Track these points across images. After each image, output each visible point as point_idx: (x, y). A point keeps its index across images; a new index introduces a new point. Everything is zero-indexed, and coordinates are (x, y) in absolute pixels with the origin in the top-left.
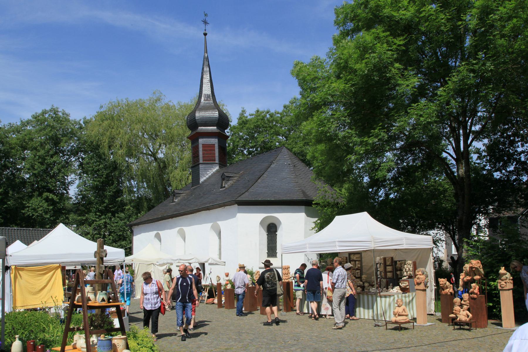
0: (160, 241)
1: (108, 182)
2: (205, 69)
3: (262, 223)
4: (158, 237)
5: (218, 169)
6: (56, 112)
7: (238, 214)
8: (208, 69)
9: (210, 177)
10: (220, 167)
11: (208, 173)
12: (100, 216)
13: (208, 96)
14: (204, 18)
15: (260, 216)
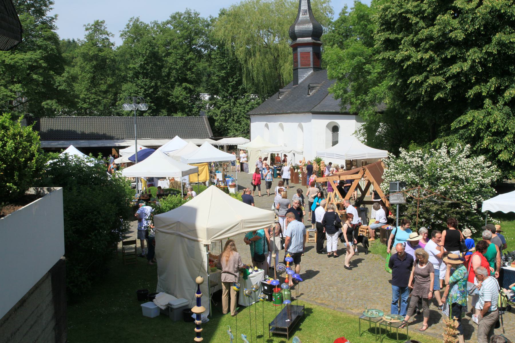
0: (268, 129)
1: (231, 74)
3: (328, 126)
4: (267, 126)
6: (189, 14)
9: (306, 79)
10: (314, 70)
12: (226, 101)
15: (327, 121)
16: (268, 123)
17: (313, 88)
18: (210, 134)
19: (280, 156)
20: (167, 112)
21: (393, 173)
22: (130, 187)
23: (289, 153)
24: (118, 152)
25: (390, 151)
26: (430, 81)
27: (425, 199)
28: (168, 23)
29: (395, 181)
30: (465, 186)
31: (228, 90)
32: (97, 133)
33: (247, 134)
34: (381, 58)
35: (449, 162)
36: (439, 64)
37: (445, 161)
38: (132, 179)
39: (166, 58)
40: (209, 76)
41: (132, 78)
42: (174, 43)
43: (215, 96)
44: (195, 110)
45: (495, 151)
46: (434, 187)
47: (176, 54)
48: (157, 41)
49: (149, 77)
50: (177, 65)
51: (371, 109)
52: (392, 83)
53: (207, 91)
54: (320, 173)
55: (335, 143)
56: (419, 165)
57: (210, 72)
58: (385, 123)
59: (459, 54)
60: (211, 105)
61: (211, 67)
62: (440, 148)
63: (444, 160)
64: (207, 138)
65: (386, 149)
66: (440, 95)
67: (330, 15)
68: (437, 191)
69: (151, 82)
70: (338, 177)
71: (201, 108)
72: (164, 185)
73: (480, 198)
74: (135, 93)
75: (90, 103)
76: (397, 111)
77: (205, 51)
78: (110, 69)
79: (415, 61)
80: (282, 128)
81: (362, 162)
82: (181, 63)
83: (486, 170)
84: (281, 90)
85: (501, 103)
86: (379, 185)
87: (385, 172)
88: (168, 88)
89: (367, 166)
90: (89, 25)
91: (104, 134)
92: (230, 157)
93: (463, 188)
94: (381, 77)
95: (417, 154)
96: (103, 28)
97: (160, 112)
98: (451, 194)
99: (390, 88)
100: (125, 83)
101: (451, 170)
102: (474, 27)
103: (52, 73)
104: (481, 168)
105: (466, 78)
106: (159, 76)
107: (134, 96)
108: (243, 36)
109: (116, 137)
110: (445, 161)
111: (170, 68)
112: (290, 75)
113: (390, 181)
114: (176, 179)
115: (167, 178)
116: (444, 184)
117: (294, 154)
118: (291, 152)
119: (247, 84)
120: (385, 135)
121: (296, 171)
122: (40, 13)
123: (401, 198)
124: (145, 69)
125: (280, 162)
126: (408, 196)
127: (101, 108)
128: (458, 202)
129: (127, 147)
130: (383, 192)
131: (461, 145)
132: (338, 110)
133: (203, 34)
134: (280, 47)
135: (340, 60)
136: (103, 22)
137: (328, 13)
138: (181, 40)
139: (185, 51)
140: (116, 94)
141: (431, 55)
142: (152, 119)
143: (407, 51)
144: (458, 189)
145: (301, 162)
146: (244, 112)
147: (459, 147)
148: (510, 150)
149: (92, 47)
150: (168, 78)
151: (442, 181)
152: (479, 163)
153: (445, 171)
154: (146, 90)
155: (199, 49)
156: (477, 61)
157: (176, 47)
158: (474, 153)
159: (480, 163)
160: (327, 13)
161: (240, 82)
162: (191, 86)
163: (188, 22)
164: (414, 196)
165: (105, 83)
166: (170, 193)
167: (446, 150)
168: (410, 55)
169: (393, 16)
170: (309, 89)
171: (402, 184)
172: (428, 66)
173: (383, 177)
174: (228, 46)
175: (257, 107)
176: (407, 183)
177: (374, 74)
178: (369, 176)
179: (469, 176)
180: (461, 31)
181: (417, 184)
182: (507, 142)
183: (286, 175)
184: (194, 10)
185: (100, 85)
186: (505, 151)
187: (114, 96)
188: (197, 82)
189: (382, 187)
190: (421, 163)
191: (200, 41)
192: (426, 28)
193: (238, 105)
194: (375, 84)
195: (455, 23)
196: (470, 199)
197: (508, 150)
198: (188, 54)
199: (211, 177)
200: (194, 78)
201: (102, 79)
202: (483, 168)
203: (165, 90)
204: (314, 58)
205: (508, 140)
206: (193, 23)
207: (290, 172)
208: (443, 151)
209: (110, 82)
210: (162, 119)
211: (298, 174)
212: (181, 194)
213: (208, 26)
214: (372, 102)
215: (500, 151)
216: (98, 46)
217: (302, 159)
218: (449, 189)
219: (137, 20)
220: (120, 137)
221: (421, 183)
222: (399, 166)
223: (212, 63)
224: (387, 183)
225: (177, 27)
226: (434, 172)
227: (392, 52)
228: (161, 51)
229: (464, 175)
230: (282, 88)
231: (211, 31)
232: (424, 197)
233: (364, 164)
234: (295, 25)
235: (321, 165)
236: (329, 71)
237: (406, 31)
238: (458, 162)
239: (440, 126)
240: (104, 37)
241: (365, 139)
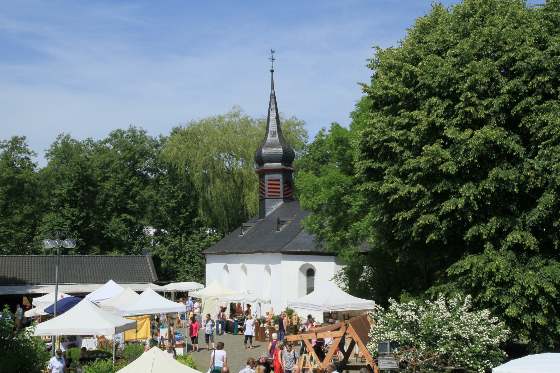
0: (228, 271)
2: (272, 106)
3: (301, 269)
4: (226, 268)
5: (283, 204)
7: (282, 261)
8: (274, 106)
9: (275, 211)
10: (284, 201)
11: (273, 207)
13: (274, 133)
14: (270, 55)
15: (301, 263)
16: (227, 264)
17: (284, 222)
18: (154, 278)
19: (242, 306)
20: (100, 249)
21: (382, 330)
22: (44, 348)
23: (254, 302)
24: (31, 301)
25: (377, 302)
26: (421, 221)
27: (422, 364)
28: (106, 141)
29: (385, 340)
30: (469, 348)
31: (180, 223)
32: (4, 276)
33: (200, 277)
34: (362, 189)
35: (449, 317)
36: (429, 199)
37: (444, 316)
38: (47, 338)
39: (102, 183)
40: (156, 204)
41: (57, 206)
42: (113, 165)
43: (162, 230)
44: (136, 247)
45: (501, 305)
46: (432, 349)
47: (116, 178)
48: (92, 163)
49: (79, 206)
50: (116, 192)
51: (352, 249)
52: (377, 219)
53: (152, 223)
54: (292, 329)
55: (310, 290)
56: (413, 320)
57: (157, 200)
58: (370, 266)
59: (452, 188)
60: (156, 241)
61: (159, 195)
62: (435, 299)
63: (442, 315)
64: (150, 282)
65: (372, 299)
66: (433, 236)
67: (303, 138)
68: (436, 354)
69: (80, 212)
70: (314, 334)
71: (144, 244)
72: (90, 345)
73: (488, 363)
74: (58, 226)
76: (384, 252)
77: (151, 175)
78: (29, 195)
79: (402, 195)
80: (245, 270)
81: (344, 314)
82: (120, 190)
83: (493, 327)
84: (244, 224)
85: (504, 248)
86: (365, 345)
87: (372, 328)
88: (104, 220)
89: (350, 320)
90: (5, 141)
91: (13, 278)
92: (179, 307)
93: (467, 350)
94: (364, 210)
95: (411, 306)
97: (92, 249)
98: (454, 358)
99: (375, 225)
100: (47, 213)
101: (452, 327)
102: (467, 159)
104: (487, 325)
105: (462, 217)
106: (91, 205)
107: (58, 230)
108: (199, 159)
109: (30, 282)
110: (444, 316)
111: (107, 196)
112: (255, 206)
113: (378, 340)
114: (107, 337)
115: (95, 336)
116: (444, 344)
117: (260, 304)
118: (256, 301)
120: (371, 281)
121: (262, 325)
123: (393, 362)
124: (74, 195)
125: (242, 313)
126: (401, 359)
127: (12, 244)
128: (463, 368)
129: (44, 294)
130: (371, 354)
131: (461, 296)
132: (314, 250)
133: (150, 155)
134: (245, 172)
135: (316, 189)
136: (24, 138)
137: (301, 136)
138: (122, 161)
139: (126, 175)
140: (34, 227)
141: (420, 189)
142: (79, 258)
143: (392, 182)
144: (462, 351)
145: (268, 314)
146: (198, 250)
147: (458, 298)
148: (519, 304)
149: (7, 168)
150: (104, 207)
151: (441, 341)
152: (483, 318)
153: (445, 329)
154: (73, 222)
155: (145, 173)
157: (116, 170)
158: (476, 307)
159: (485, 318)
160: (300, 136)
161: (194, 213)
163: (132, 141)
164: (408, 360)
165: (21, 212)
166: (97, 356)
167: (444, 302)
168: (396, 187)
169: (375, 143)
170: (279, 223)
171: (394, 344)
172: (417, 201)
173: (370, 335)
175: (213, 244)
176: (399, 343)
177: (355, 207)
178: (352, 334)
179: (474, 335)
180: (453, 163)
181: (411, 345)
182: (514, 294)
183: (250, 330)
184: (141, 128)
185: (14, 215)
186: (513, 304)
187: (32, 229)
188: (140, 213)
189: (370, 347)
190: (415, 317)
191: (147, 163)
192: (412, 158)
193: (191, 241)
194: (357, 218)
195: (446, 154)
196: (476, 364)
197: (516, 304)
198: (130, 178)
199: (153, 334)
200: (137, 209)
201: (16, 208)
202: (490, 325)
203: (98, 222)
204: (284, 187)
205: (515, 292)
206: (137, 143)
207: (254, 327)
208: (441, 303)
209: (28, 211)
210: (93, 258)
211: (264, 329)
212: (112, 359)
213: (157, 146)
214: (355, 240)
215: (507, 305)
216: (16, 167)
217: (269, 311)
218: (450, 351)
219: (68, 137)
220: (36, 282)
221: (416, 343)
222: (388, 321)
223: (159, 190)
224: (375, 342)
225: (118, 147)
226: (432, 330)
227: (376, 182)
228: (96, 175)
229: (468, 333)
230: (245, 222)
231: (160, 152)
232: (421, 361)
233: (346, 318)
234: (262, 148)
235: (294, 317)
236: (302, 201)
237: (390, 159)
238: (459, 317)
239: (436, 272)
240: (23, 156)
241: (346, 285)
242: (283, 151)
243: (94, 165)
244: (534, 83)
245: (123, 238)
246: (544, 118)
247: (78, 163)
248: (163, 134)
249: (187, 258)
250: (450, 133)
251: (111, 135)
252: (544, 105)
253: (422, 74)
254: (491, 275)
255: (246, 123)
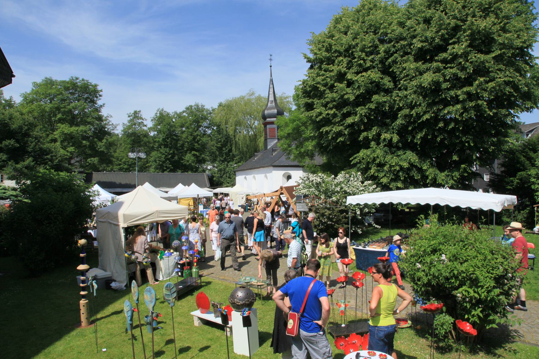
0: (267, 178)
1: (224, 145)
3: (284, 175)
6: (198, 106)
12: (222, 163)
14: (269, 57)
15: (283, 172)
17: (275, 150)
28: (184, 112)
41: (158, 148)
64: (206, 187)
66: (341, 139)
75: (128, 165)
82: (190, 138)
90: (130, 113)
96: (140, 115)
98: (341, 203)
103: (96, 140)
119: (235, 151)
122: (93, 102)
124: (166, 142)
136: (140, 111)
154: (166, 156)
156: (363, 114)
161: (230, 150)
162: (197, 153)
174: (223, 126)
198: (196, 132)
213: (210, 113)
219: (163, 110)
240: (140, 121)
242: (277, 111)
243: (177, 125)
244: (398, 45)
245: (193, 164)
246: (404, 65)
247: (167, 124)
248: (213, 107)
249: (228, 175)
250: (349, 76)
251: (186, 109)
252: (404, 58)
253: (335, 45)
254: (374, 159)
255: (259, 98)
